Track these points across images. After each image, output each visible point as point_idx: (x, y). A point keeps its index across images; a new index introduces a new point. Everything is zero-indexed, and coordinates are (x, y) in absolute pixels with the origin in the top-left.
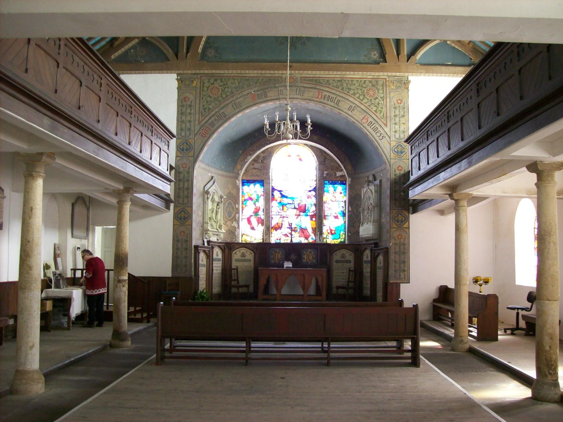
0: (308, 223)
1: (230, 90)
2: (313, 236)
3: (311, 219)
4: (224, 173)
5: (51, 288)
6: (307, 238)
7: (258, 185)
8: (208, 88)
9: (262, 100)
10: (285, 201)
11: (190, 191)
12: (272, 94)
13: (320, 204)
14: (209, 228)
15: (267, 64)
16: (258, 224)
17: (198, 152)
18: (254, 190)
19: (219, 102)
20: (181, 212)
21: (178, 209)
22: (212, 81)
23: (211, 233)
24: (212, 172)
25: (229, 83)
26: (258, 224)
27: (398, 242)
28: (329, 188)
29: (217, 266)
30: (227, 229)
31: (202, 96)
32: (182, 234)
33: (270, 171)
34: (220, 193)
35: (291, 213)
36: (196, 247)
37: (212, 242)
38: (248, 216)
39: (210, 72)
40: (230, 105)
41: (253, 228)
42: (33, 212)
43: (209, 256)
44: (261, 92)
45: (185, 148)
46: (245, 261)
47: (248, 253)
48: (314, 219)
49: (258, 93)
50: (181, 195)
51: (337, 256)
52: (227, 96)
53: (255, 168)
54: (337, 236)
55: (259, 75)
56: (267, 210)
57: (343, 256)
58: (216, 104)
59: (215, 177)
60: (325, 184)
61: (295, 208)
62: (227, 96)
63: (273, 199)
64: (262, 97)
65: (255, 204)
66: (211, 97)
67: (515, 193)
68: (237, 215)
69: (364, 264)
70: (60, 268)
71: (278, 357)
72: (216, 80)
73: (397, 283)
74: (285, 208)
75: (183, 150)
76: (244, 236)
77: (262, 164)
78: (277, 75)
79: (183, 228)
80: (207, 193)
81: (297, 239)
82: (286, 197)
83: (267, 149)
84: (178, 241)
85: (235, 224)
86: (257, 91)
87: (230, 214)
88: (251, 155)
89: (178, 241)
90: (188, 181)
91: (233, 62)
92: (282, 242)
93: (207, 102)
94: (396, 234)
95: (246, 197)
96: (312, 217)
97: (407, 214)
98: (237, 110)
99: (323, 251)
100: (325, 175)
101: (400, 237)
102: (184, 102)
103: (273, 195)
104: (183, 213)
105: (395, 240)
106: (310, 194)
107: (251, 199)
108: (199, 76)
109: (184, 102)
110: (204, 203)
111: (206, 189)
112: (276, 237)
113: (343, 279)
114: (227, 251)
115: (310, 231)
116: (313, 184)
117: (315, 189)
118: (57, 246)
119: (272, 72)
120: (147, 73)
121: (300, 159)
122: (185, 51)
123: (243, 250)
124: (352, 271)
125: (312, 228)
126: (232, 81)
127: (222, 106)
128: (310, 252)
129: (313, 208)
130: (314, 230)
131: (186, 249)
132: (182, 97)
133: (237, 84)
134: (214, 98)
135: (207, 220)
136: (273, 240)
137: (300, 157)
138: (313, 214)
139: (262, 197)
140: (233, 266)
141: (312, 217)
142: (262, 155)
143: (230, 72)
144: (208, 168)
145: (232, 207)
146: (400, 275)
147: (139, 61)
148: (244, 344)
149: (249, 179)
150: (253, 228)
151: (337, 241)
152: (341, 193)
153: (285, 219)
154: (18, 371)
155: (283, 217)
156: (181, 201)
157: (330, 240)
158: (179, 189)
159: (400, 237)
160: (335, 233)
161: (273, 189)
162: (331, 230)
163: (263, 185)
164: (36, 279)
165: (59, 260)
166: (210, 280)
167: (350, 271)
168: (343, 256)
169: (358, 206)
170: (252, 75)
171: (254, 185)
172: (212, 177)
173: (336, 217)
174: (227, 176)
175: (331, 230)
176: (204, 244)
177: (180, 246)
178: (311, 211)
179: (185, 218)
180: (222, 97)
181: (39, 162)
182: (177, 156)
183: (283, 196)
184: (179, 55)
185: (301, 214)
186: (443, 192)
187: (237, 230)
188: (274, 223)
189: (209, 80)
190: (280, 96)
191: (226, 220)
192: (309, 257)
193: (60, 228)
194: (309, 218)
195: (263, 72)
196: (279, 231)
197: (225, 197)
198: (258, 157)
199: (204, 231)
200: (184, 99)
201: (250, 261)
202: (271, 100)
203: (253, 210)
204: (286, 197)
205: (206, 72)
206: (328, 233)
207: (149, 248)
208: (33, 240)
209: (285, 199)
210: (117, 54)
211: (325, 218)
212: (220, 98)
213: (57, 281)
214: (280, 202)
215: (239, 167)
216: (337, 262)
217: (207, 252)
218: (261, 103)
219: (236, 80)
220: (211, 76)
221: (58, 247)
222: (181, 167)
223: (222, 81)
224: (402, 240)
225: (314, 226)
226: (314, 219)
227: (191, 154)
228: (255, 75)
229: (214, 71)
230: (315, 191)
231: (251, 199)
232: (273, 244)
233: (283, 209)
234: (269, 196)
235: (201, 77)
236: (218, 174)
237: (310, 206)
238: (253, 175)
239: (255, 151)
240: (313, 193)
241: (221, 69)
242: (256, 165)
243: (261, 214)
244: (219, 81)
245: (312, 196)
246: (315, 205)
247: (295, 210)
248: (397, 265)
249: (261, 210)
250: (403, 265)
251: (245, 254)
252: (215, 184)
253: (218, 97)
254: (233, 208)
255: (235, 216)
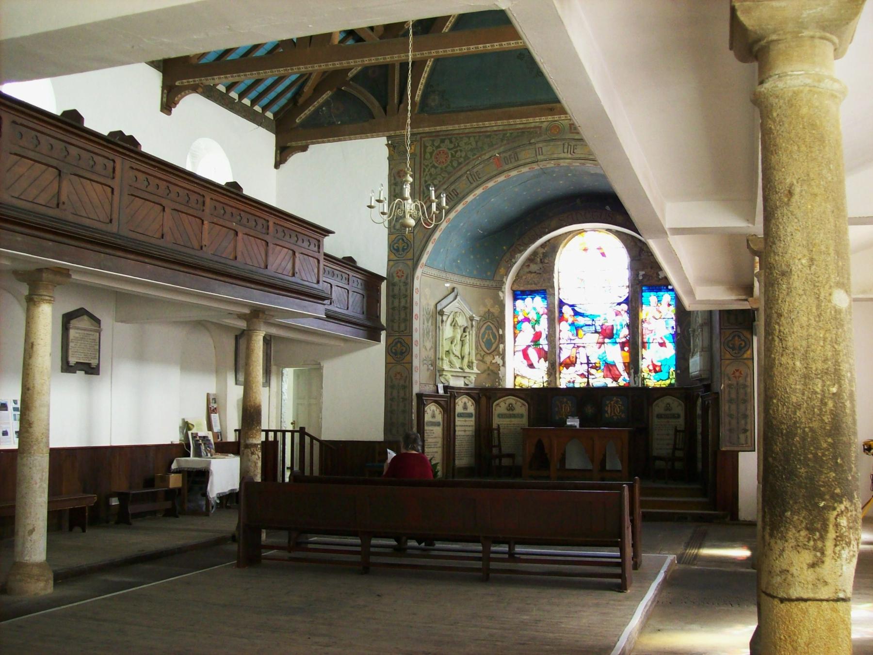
0: (616, 355)
1: (463, 154)
2: (625, 375)
3: (623, 349)
4: (483, 283)
5: (189, 456)
6: (615, 379)
7: (538, 299)
8: (431, 154)
9: (511, 166)
10: (581, 321)
11: (408, 310)
12: (526, 155)
13: (634, 325)
14: (446, 367)
15: (516, 108)
16: (540, 358)
17: (418, 253)
18: (534, 306)
19: (449, 173)
20: (396, 343)
21: (393, 338)
22: (436, 144)
23: (449, 375)
24: (452, 281)
25: (462, 144)
26: (540, 358)
27: (735, 383)
28: (651, 298)
29: (465, 427)
30: (484, 367)
31: (423, 167)
32: (398, 376)
33: (556, 275)
34: (469, 313)
35: (590, 339)
36: (420, 396)
37: (453, 388)
38: (524, 347)
39: (432, 129)
40: (465, 178)
41: (531, 366)
42: (35, 348)
43: (448, 409)
44: (509, 153)
45: (401, 247)
46: (514, 416)
47: (519, 404)
48: (626, 349)
49: (505, 154)
50: (397, 318)
51: (659, 407)
52: (459, 164)
53: (530, 272)
54: (663, 375)
55: (506, 128)
56: (552, 337)
57: (668, 407)
58: (444, 178)
59: (460, 288)
60: (642, 291)
61: (596, 332)
62: (459, 164)
63: (561, 318)
64: (512, 159)
65: (533, 327)
66: (436, 167)
67: (864, 292)
68: (501, 346)
69: (457, 419)
70: (217, 428)
71: (538, 570)
72: (443, 141)
73: (733, 451)
74: (581, 332)
75: (397, 250)
76: (518, 378)
77: (541, 265)
78: (533, 125)
79: (399, 368)
80: (441, 313)
81: (599, 380)
82: (582, 315)
83: (549, 241)
84: (393, 387)
85: (498, 360)
86: (504, 152)
87: (489, 344)
88: (521, 252)
89: (393, 387)
90: (406, 296)
91: (467, 111)
92: (577, 385)
93: (431, 175)
94: (730, 370)
95: (521, 317)
96: (623, 345)
97: (749, 336)
98: (475, 185)
99: (638, 397)
100: (641, 278)
101: (737, 374)
102: (397, 178)
103: (561, 312)
104: (399, 345)
105: (729, 379)
106: (619, 308)
107: (527, 320)
108: (419, 136)
109: (397, 178)
110: (436, 328)
111: (439, 308)
112: (567, 378)
113: (668, 444)
114: (484, 400)
115: (621, 367)
116: (625, 293)
117: (626, 301)
118: (211, 398)
119: (524, 120)
120: (345, 140)
121: (603, 254)
122: (396, 101)
123: (511, 400)
124: (680, 431)
125: (624, 363)
126: (466, 140)
127: (452, 179)
128: (617, 402)
129: (626, 331)
130: (627, 367)
131: (404, 399)
132: (395, 171)
133: (474, 144)
134: (441, 169)
135: (441, 353)
136: (563, 383)
137: (601, 251)
138: (624, 340)
139: (545, 317)
140: (495, 426)
141: (623, 345)
142: (542, 251)
143: (462, 126)
144: (444, 275)
145: (493, 333)
146: (739, 438)
147: (334, 123)
148: (479, 547)
149: (522, 289)
150: (531, 366)
151: (665, 384)
152: (669, 305)
153: (581, 349)
154: (15, 563)
155: (578, 347)
156: (396, 328)
157: (652, 382)
158: (393, 309)
159: (737, 374)
160: (661, 371)
161: (561, 304)
162: (654, 366)
163: (545, 298)
164: (37, 440)
165: (215, 417)
166: (452, 449)
167: (676, 431)
168: (668, 407)
169: (689, 325)
170: (495, 128)
171: (533, 299)
172: (453, 289)
173: (662, 345)
174: (480, 287)
175: (654, 366)
176: (438, 392)
177: (395, 392)
178: (622, 335)
179: (402, 353)
180: (452, 166)
181: (41, 281)
182: (389, 260)
183: (576, 313)
184: (388, 107)
185: (607, 340)
186: (734, 297)
187: (502, 368)
188: (563, 356)
189: (433, 141)
190: (539, 157)
191: (483, 353)
192: (614, 409)
193: (218, 371)
194: (618, 346)
195: (511, 121)
196: (571, 368)
197: (478, 319)
198: (535, 253)
199: (437, 372)
200: (399, 173)
201: (522, 416)
202: (524, 165)
203: (531, 337)
204: (582, 315)
205: (427, 129)
206: (650, 371)
207: (350, 397)
208: (34, 387)
209: (580, 318)
210: (303, 116)
211: (644, 347)
212: (450, 169)
213: (197, 446)
214: (573, 324)
215: (502, 270)
216: (659, 416)
217: (442, 403)
218: (509, 170)
219: (472, 139)
220: (436, 136)
221: (214, 399)
222: (395, 275)
223: (451, 142)
224: (741, 381)
225: (628, 360)
226: (626, 349)
227: (410, 255)
228: (501, 128)
229: (438, 128)
230: (627, 304)
231: (527, 320)
232: (563, 389)
233: (577, 335)
234: (555, 315)
235: (421, 138)
236: (461, 283)
237: (619, 327)
238: (528, 283)
239: (527, 246)
240: (625, 307)
241: (448, 124)
242: (534, 267)
243: (544, 342)
244: (447, 142)
245: (623, 313)
246: (628, 326)
247: (597, 335)
248: (734, 422)
249: (544, 336)
250: (743, 422)
251: (514, 405)
252: (458, 298)
253: (446, 167)
254: (494, 337)
255: (498, 346)
